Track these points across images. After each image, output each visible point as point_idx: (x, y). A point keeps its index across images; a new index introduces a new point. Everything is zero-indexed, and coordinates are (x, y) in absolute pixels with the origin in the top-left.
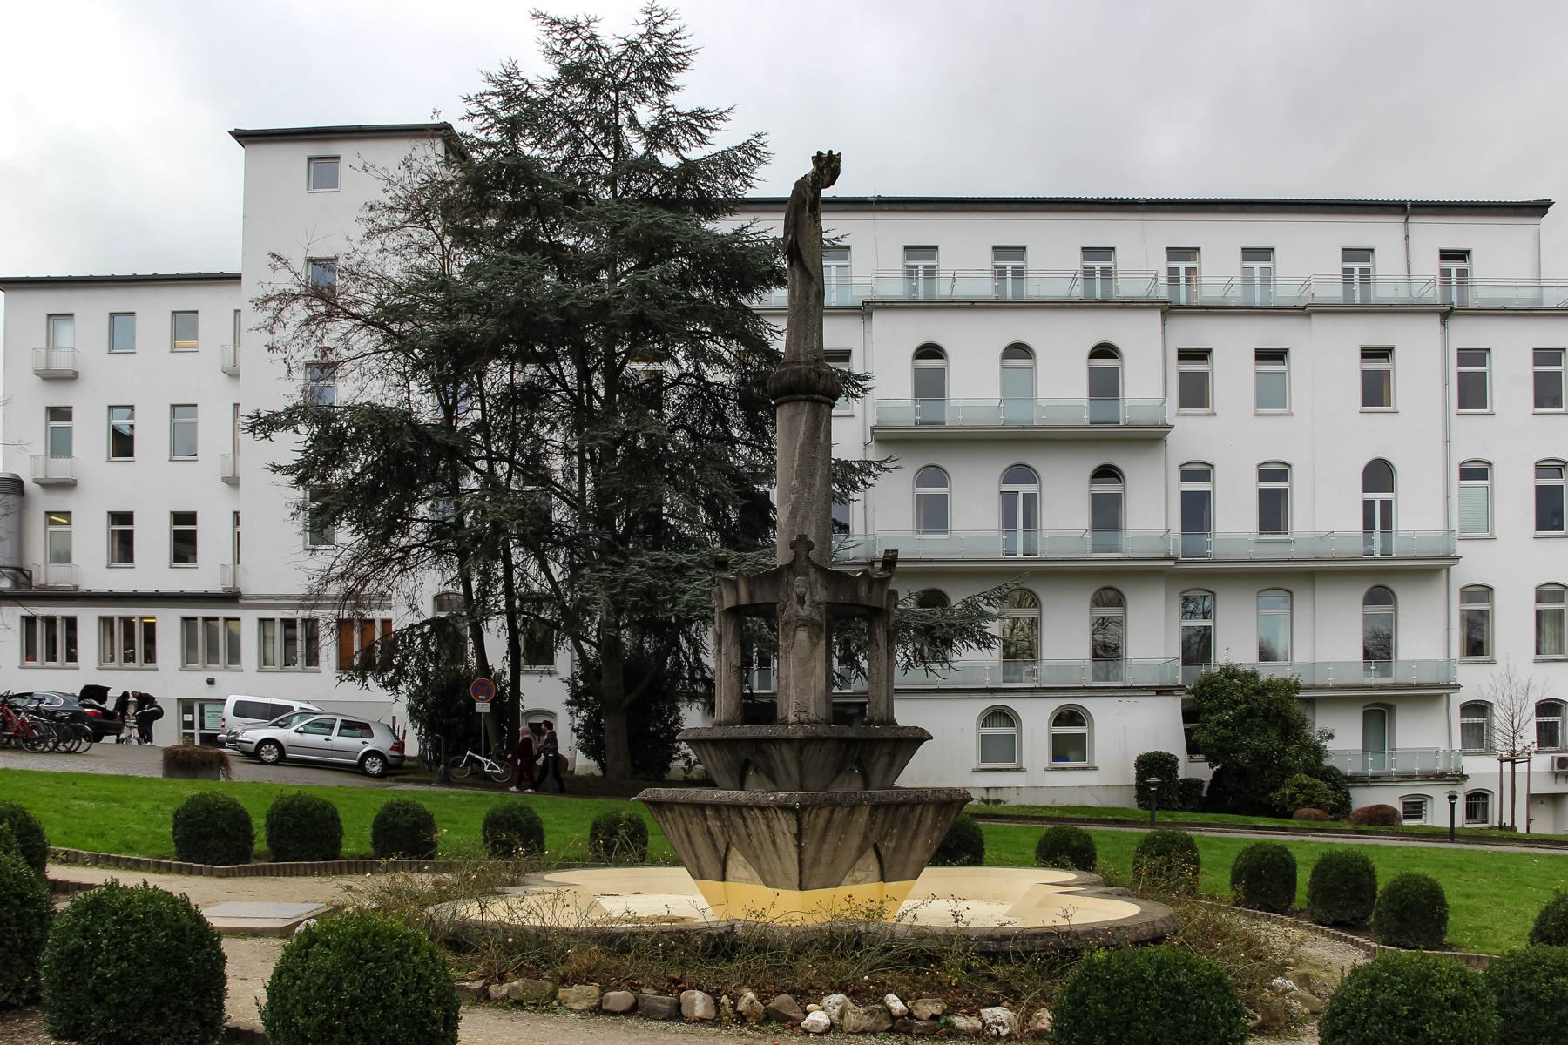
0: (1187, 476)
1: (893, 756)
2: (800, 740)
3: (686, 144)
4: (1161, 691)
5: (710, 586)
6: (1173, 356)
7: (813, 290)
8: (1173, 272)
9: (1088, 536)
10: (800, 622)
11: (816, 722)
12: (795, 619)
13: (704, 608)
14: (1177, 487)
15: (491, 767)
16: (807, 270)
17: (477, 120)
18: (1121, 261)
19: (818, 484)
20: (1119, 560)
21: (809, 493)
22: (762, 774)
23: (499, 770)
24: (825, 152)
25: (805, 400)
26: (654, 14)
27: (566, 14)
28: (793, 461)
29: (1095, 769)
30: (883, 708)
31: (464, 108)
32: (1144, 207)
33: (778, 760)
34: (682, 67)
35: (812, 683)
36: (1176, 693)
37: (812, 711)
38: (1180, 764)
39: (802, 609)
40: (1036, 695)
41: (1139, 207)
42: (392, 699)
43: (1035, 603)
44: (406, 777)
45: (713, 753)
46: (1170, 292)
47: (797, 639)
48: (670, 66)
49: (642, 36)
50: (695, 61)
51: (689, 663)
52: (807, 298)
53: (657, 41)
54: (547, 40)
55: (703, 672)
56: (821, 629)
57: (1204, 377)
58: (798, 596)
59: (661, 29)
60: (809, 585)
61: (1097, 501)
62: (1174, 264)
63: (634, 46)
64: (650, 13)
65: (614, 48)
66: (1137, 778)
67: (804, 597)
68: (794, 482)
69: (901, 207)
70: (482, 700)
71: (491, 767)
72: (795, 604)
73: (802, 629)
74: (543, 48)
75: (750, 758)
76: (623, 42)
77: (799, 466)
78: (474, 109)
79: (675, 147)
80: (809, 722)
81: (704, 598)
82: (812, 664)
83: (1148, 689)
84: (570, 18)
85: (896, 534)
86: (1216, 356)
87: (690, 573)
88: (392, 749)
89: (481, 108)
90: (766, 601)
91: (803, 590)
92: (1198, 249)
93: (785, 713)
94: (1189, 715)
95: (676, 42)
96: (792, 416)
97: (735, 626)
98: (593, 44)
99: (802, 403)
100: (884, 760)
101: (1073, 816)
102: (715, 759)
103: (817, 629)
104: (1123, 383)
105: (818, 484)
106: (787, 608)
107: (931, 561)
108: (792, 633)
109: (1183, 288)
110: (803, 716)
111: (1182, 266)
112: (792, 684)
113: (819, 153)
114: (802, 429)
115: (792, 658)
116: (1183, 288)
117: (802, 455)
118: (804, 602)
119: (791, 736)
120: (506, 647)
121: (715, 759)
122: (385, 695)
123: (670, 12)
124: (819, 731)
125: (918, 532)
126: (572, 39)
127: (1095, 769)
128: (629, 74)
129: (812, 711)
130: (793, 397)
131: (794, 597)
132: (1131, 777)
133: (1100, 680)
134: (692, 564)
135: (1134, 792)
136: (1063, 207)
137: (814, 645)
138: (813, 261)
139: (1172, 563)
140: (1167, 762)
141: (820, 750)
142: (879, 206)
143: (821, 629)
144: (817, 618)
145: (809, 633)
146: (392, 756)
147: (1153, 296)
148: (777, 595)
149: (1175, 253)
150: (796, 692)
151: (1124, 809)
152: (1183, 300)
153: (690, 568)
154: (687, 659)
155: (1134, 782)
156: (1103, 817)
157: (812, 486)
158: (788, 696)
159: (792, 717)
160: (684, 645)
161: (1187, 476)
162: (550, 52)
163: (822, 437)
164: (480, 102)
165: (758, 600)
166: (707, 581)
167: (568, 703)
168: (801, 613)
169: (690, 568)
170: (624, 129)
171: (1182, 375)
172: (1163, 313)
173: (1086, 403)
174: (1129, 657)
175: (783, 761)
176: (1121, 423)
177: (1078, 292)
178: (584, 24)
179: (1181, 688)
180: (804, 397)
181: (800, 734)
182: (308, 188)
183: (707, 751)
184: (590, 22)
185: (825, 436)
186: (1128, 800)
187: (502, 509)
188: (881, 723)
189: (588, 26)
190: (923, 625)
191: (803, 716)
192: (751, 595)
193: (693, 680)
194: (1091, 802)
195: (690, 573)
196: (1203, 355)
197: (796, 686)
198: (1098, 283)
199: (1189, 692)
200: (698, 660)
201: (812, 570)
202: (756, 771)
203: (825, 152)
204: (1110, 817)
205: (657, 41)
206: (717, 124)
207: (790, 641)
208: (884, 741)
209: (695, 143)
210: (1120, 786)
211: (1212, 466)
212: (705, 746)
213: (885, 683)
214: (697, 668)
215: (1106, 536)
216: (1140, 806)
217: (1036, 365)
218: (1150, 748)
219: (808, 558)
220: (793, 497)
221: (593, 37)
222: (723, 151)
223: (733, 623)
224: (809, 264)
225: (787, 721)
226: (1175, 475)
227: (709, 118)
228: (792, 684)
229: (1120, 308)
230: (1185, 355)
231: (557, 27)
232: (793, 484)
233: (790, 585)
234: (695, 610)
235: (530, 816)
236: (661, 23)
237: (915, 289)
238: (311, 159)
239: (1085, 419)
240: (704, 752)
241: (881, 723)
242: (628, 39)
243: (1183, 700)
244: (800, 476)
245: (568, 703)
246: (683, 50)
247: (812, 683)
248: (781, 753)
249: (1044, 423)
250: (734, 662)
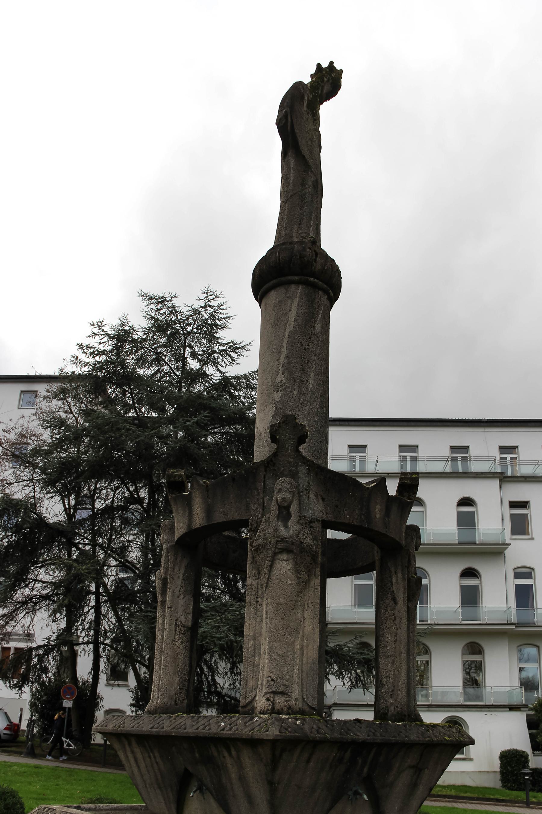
0: (517, 575)
1: (418, 770)
2: (274, 742)
3: (223, 364)
4: (512, 708)
5: (218, 623)
6: (507, 505)
7: (310, 180)
8: (503, 459)
9: (460, 610)
10: (281, 545)
11: (302, 712)
12: (273, 541)
13: (212, 637)
14: (513, 582)
15: (69, 745)
16: (304, 157)
17: (97, 337)
18: (473, 452)
19: (311, 381)
20: (480, 624)
21: (300, 389)
22: (208, 795)
23: (73, 747)
24: (325, 65)
25: (298, 283)
26: (209, 294)
27: (157, 292)
28: (279, 353)
29: (471, 760)
30: (402, 694)
31: (89, 330)
32: (485, 424)
33: (234, 776)
34: (224, 327)
35: (297, 646)
36: (522, 709)
37: (296, 693)
38: (530, 758)
39: (286, 526)
40: (431, 709)
41: (482, 424)
42: (17, 696)
43: (427, 651)
44: (9, 749)
45: (139, 756)
46: (502, 469)
47: (273, 573)
48: (217, 326)
49: (202, 307)
50: (231, 323)
51: (208, 682)
52: (303, 184)
53: (210, 310)
54: (146, 309)
55: (216, 687)
56: (314, 558)
57: (525, 518)
58: (280, 507)
59: (212, 303)
60: (298, 493)
61: (464, 589)
62: (504, 455)
63: (195, 311)
64: (207, 293)
65: (185, 311)
66: (501, 767)
67: (288, 508)
68: (280, 377)
69: (347, 423)
70: (68, 699)
71: (69, 745)
72: (273, 520)
73: (285, 557)
74: (145, 314)
75: (190, 768)
76: (190, 309)
77: (287, 357)
78: (96, 330)
79: (216, 364)
80: (290, 711)
81: (214, 630)
82: (299, 615)
83: (504, 706)
84: (161, 295)
85: (342, 608)
86: (532, 505)
87: (206, 615)
88: (5, 729)
89: (101, 330)
90: (230, 518)
91: (288, 496)
92: (517, 447)
93: (250, 696)
94: (531, 724)
95: (221, 311)
96: (280, 302)
97: (186, 568)
98: (174, 311)
99: (293, 287)
100: (406, 777)
101: (466, 795)
102: (142, 765)
103: (309, 559)
104: (478, 520)
105: (311, 381)
106: (262, 526)
107: (363, 624)
108: (267, 563)
109: (509, 467)
110: (280, 701)
111: (508, 456)
112: (265, 645)
113: (319, 65)
114: (293, 314)
115: (267, 605)
116: (509, 467)
117: (291, 345)
118: (289, 516)
119: (257, 735)
120: (91, 666)
121: (142, 765)
122: (13, 694)
123: (218, 293)
124: (307, 727)
125: (355, 606)
126: (161, 309)
127: (471, 760)
128: (193, 329)
129: (296, 693)
130: (283, 279)
131: (274, 508)
132: (496, 765)
133: (470, 700)
134: (208, 609)
135: (499, 777)
136: (439, 424)
137: (303, 585)
138: (311, 153)
139: (513, 627)
140: (522, 756)
141: (308, 761)
142: (334, 423)
143: (314, 558)
144: (309, 541)
145: (296, 564)
146: (4, 734)
147: (493, 471)
148: (248, 508)
149: (503, 449)
150: (271, 660)
151: (494, 789)
152: (510, 474)
153: (206, 611)
154: (207, 679)
155: (498, 769)
156: (487, 796)
157: (303, 382)
158: (256, 667)
159: (261, 703)
160: (205, 669)
161: (517, 575)
162: (149, 317)
163: (318, 327)
164: (99, 326)
165: (219, 518)
166: (217, 620)
167: (131, 705)
168: (284, 532)
169: (206, 611)
170: (188, 359)
171: (512, 516)
172: (500, 481)
173: (456, 531)
174: (487, 685)
175: (242, 778)
176: (477, 543)
177: (448, 470)
178: (168, 299)
179: (526, 706)
180: (296, 278)
181: (273, 732)
182: (19, 406)
183: (133, 752)
184: (172, 297)
185: (322, 328)
186: (495, 782)
187: (84, 567)
188: (400, 717)
189: (171, 300)
190: (363, 658)
191: (280, 701)
192: (209, 512)
193: (209, 692)
194: (469, 782)
195: (206, 615)
196: (524, 505)
197: (271, 650)
198: (460, 463)
199: (531, 709)
200: (214, 680)
201: (303, 470)
202: (200, 789)
203: (325, 65)
204: (492, 797)
205: (210, 310)
206: (244, 352)
207: (264, 576)
208: (409, 746)
209: (228, 364)
210: (488, 772)
211: (533, 569)
212: (130, 744)
213: (404, 655)
214: (213, 685)
215: (470, 609)
216: (503, 786)
217: (425, 510)
218: (508, 747)
219: (298, 451)
220: (277, 396)
221: (174, 307)
222: (245, 374)
223: (185, 562)
224: (305, 152)
225: (253, 709)
226: (511, 575)
227: (237, 348)
228: (265, 645)
229: (475, 477)
230: (514, 505)
231: (153, 301)
232: (278, 380)
233: (268, 492)
234: (207, 639)
235: (10, 801)
236: (213, 299)
237: (355, 466)
238: (22, 392)
239: (456, 540)
240: (128, 748)
241: (400, 717)
242: (193, 307)
243: (527, 715)
244: (288, 369)
245: (131, 705)
246: (225, 316)
247: (297, 646)
248: (240, 767)
249: (432, 542)
250: (182, 619)
